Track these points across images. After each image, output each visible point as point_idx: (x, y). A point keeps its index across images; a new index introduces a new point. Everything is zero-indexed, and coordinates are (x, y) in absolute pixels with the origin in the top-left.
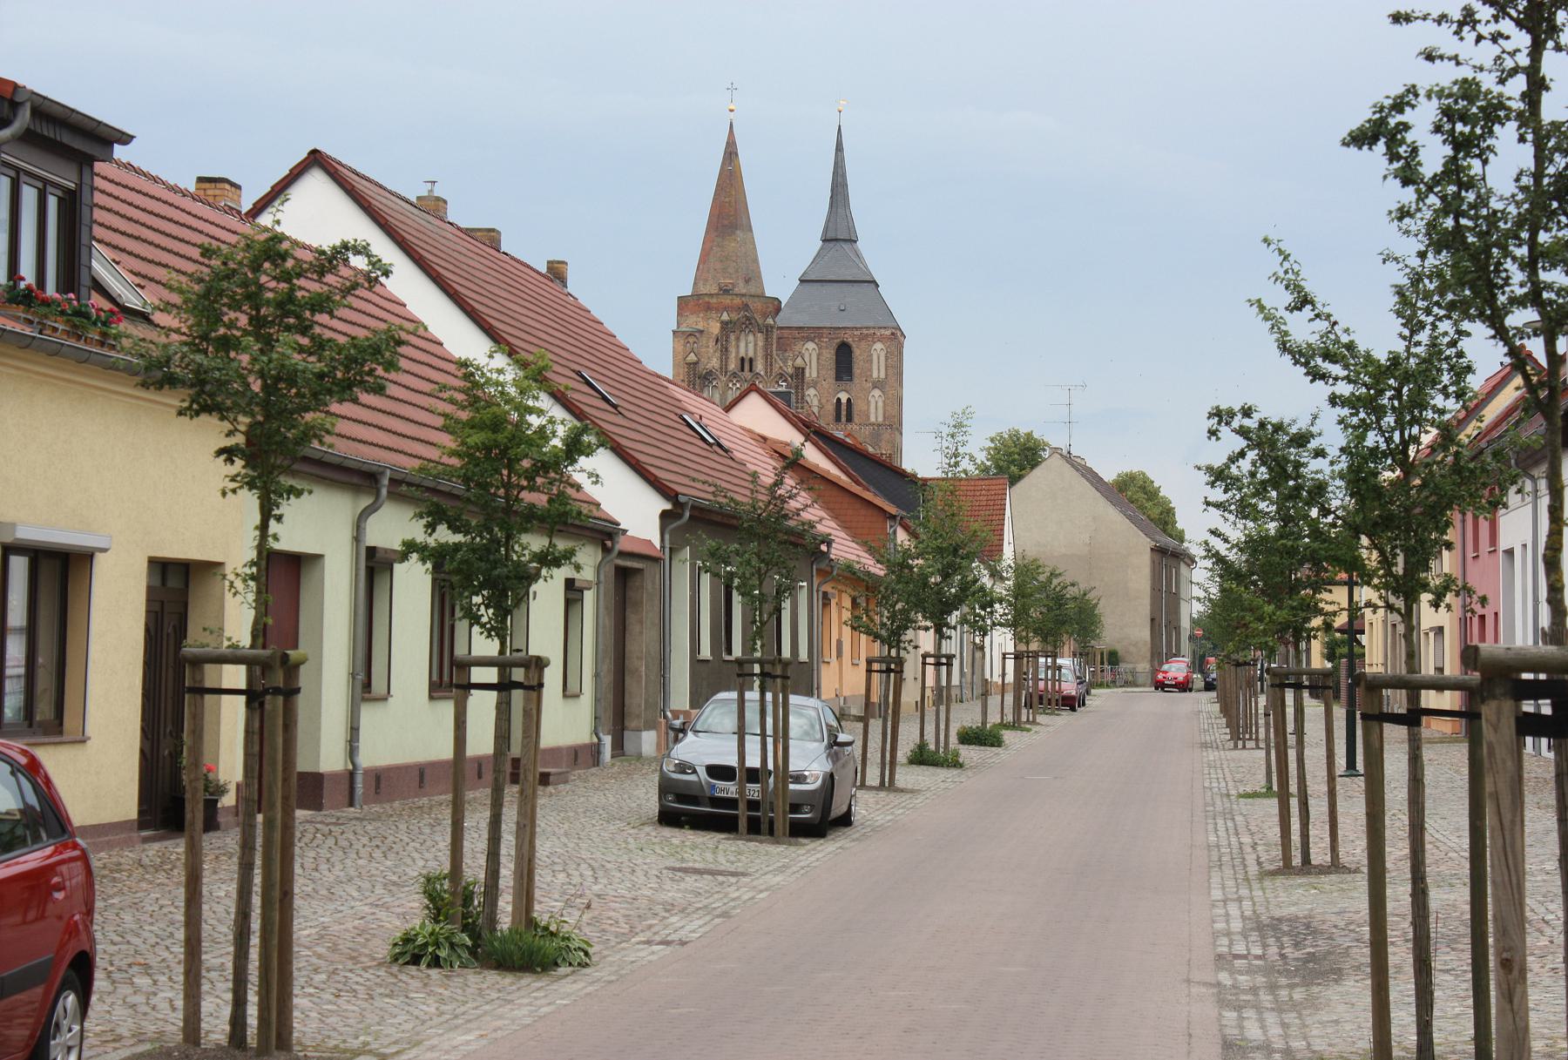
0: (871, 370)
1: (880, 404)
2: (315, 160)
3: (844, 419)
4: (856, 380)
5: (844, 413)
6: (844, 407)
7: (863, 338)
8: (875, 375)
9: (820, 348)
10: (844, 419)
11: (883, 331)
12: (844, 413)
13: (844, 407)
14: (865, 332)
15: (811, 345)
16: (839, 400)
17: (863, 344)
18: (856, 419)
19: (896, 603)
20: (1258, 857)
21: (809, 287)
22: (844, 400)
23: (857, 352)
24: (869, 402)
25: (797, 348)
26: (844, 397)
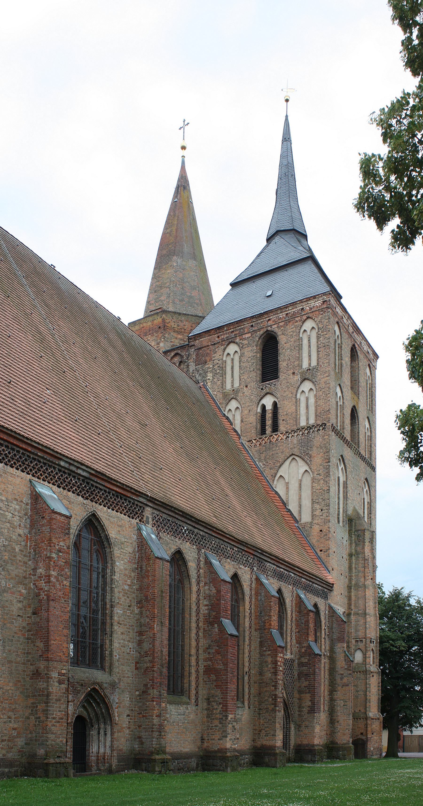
0: (300, 359)
1: (312, 401)
2: (359, 649)
3: (269, 430)
4: (282, 376)
5: (269, 422)
6: (269, 416)
7: (290, 319)
8: (305, 365)
9: (241, 348)
10: (269, 430)
11: (312, 303)
12: (269, 422)
13: (269, 416)
14: (291, 311)
15: (232, 348)
16: (264, 407)
17: (290, 328)
18: (282, 427)
19: (365, 657)
20: (212, 345)
21: (243, 289)
22: (269, 407)
23: (282, 339)
24: (297, 402)
25: (217, 356)
26: (268, 402)
